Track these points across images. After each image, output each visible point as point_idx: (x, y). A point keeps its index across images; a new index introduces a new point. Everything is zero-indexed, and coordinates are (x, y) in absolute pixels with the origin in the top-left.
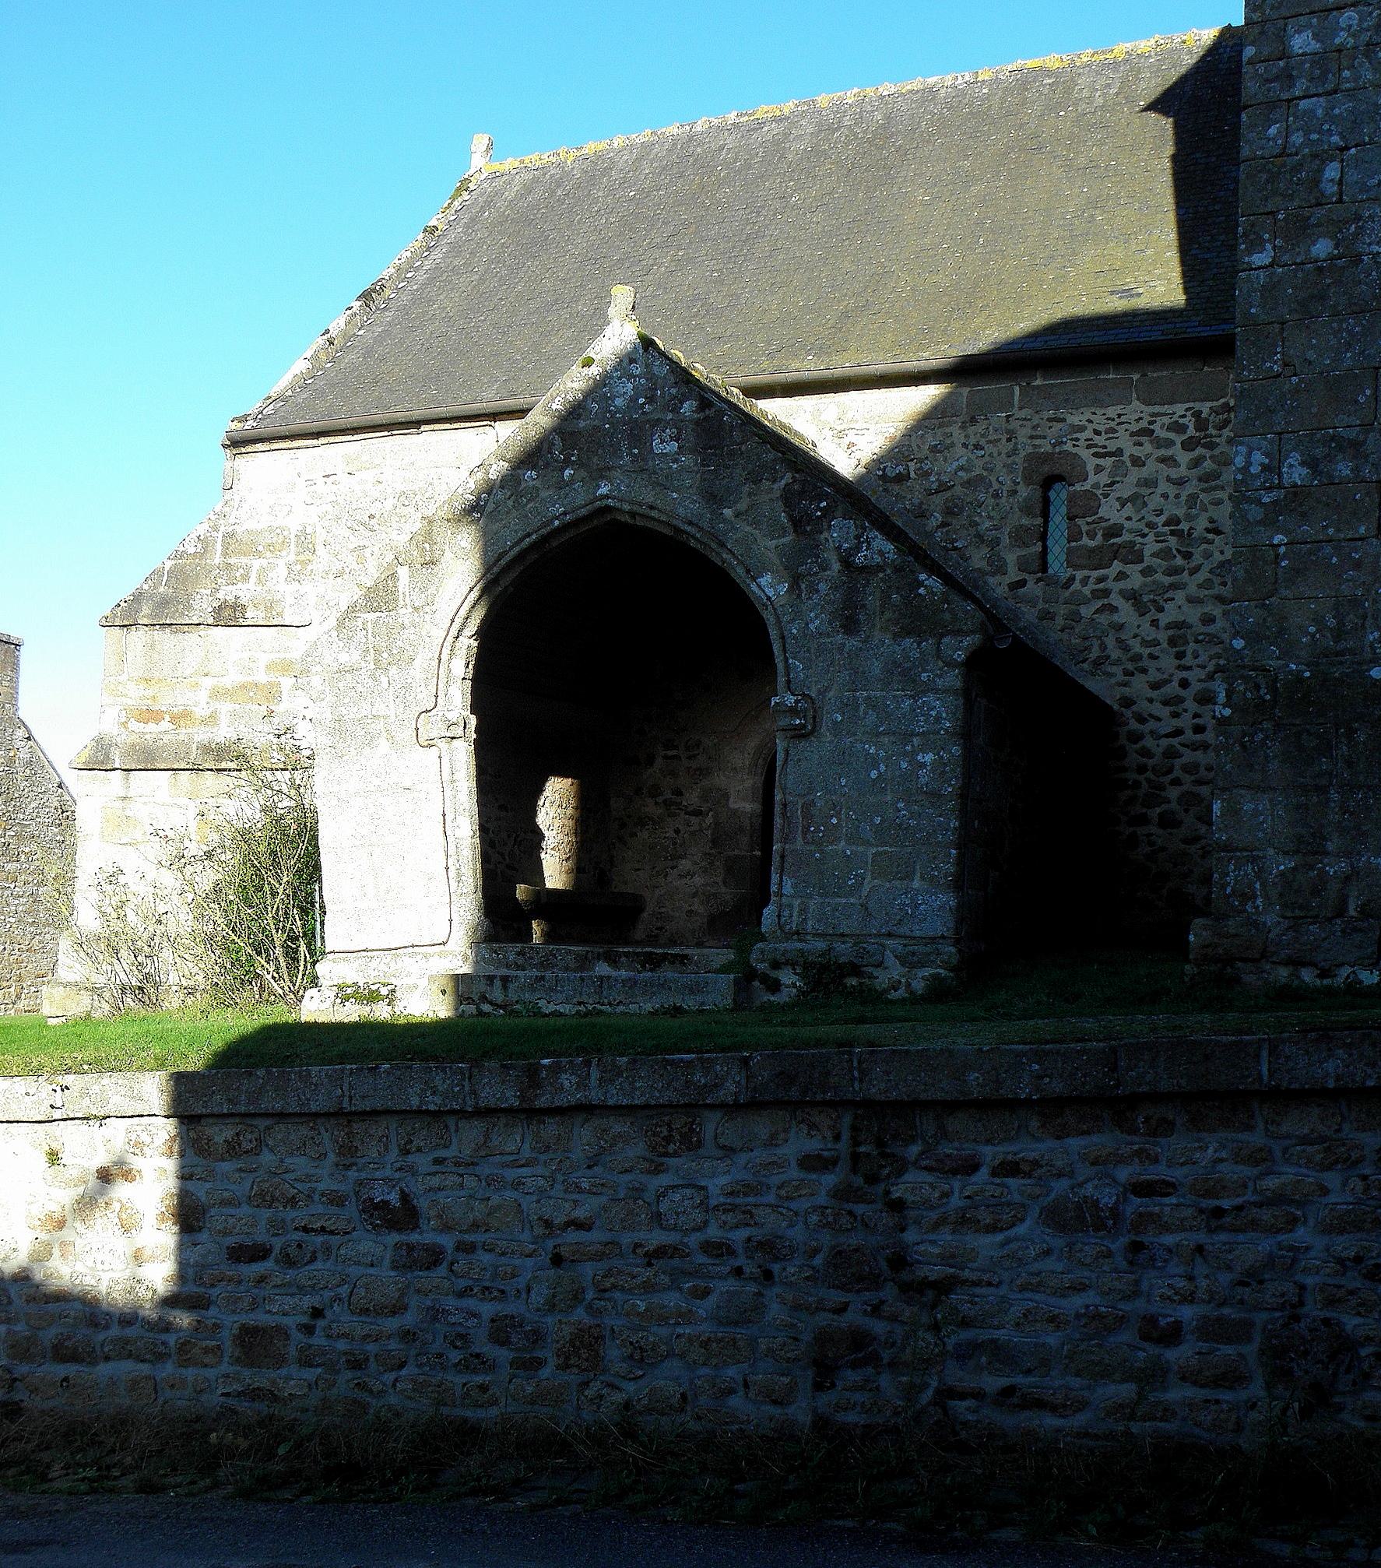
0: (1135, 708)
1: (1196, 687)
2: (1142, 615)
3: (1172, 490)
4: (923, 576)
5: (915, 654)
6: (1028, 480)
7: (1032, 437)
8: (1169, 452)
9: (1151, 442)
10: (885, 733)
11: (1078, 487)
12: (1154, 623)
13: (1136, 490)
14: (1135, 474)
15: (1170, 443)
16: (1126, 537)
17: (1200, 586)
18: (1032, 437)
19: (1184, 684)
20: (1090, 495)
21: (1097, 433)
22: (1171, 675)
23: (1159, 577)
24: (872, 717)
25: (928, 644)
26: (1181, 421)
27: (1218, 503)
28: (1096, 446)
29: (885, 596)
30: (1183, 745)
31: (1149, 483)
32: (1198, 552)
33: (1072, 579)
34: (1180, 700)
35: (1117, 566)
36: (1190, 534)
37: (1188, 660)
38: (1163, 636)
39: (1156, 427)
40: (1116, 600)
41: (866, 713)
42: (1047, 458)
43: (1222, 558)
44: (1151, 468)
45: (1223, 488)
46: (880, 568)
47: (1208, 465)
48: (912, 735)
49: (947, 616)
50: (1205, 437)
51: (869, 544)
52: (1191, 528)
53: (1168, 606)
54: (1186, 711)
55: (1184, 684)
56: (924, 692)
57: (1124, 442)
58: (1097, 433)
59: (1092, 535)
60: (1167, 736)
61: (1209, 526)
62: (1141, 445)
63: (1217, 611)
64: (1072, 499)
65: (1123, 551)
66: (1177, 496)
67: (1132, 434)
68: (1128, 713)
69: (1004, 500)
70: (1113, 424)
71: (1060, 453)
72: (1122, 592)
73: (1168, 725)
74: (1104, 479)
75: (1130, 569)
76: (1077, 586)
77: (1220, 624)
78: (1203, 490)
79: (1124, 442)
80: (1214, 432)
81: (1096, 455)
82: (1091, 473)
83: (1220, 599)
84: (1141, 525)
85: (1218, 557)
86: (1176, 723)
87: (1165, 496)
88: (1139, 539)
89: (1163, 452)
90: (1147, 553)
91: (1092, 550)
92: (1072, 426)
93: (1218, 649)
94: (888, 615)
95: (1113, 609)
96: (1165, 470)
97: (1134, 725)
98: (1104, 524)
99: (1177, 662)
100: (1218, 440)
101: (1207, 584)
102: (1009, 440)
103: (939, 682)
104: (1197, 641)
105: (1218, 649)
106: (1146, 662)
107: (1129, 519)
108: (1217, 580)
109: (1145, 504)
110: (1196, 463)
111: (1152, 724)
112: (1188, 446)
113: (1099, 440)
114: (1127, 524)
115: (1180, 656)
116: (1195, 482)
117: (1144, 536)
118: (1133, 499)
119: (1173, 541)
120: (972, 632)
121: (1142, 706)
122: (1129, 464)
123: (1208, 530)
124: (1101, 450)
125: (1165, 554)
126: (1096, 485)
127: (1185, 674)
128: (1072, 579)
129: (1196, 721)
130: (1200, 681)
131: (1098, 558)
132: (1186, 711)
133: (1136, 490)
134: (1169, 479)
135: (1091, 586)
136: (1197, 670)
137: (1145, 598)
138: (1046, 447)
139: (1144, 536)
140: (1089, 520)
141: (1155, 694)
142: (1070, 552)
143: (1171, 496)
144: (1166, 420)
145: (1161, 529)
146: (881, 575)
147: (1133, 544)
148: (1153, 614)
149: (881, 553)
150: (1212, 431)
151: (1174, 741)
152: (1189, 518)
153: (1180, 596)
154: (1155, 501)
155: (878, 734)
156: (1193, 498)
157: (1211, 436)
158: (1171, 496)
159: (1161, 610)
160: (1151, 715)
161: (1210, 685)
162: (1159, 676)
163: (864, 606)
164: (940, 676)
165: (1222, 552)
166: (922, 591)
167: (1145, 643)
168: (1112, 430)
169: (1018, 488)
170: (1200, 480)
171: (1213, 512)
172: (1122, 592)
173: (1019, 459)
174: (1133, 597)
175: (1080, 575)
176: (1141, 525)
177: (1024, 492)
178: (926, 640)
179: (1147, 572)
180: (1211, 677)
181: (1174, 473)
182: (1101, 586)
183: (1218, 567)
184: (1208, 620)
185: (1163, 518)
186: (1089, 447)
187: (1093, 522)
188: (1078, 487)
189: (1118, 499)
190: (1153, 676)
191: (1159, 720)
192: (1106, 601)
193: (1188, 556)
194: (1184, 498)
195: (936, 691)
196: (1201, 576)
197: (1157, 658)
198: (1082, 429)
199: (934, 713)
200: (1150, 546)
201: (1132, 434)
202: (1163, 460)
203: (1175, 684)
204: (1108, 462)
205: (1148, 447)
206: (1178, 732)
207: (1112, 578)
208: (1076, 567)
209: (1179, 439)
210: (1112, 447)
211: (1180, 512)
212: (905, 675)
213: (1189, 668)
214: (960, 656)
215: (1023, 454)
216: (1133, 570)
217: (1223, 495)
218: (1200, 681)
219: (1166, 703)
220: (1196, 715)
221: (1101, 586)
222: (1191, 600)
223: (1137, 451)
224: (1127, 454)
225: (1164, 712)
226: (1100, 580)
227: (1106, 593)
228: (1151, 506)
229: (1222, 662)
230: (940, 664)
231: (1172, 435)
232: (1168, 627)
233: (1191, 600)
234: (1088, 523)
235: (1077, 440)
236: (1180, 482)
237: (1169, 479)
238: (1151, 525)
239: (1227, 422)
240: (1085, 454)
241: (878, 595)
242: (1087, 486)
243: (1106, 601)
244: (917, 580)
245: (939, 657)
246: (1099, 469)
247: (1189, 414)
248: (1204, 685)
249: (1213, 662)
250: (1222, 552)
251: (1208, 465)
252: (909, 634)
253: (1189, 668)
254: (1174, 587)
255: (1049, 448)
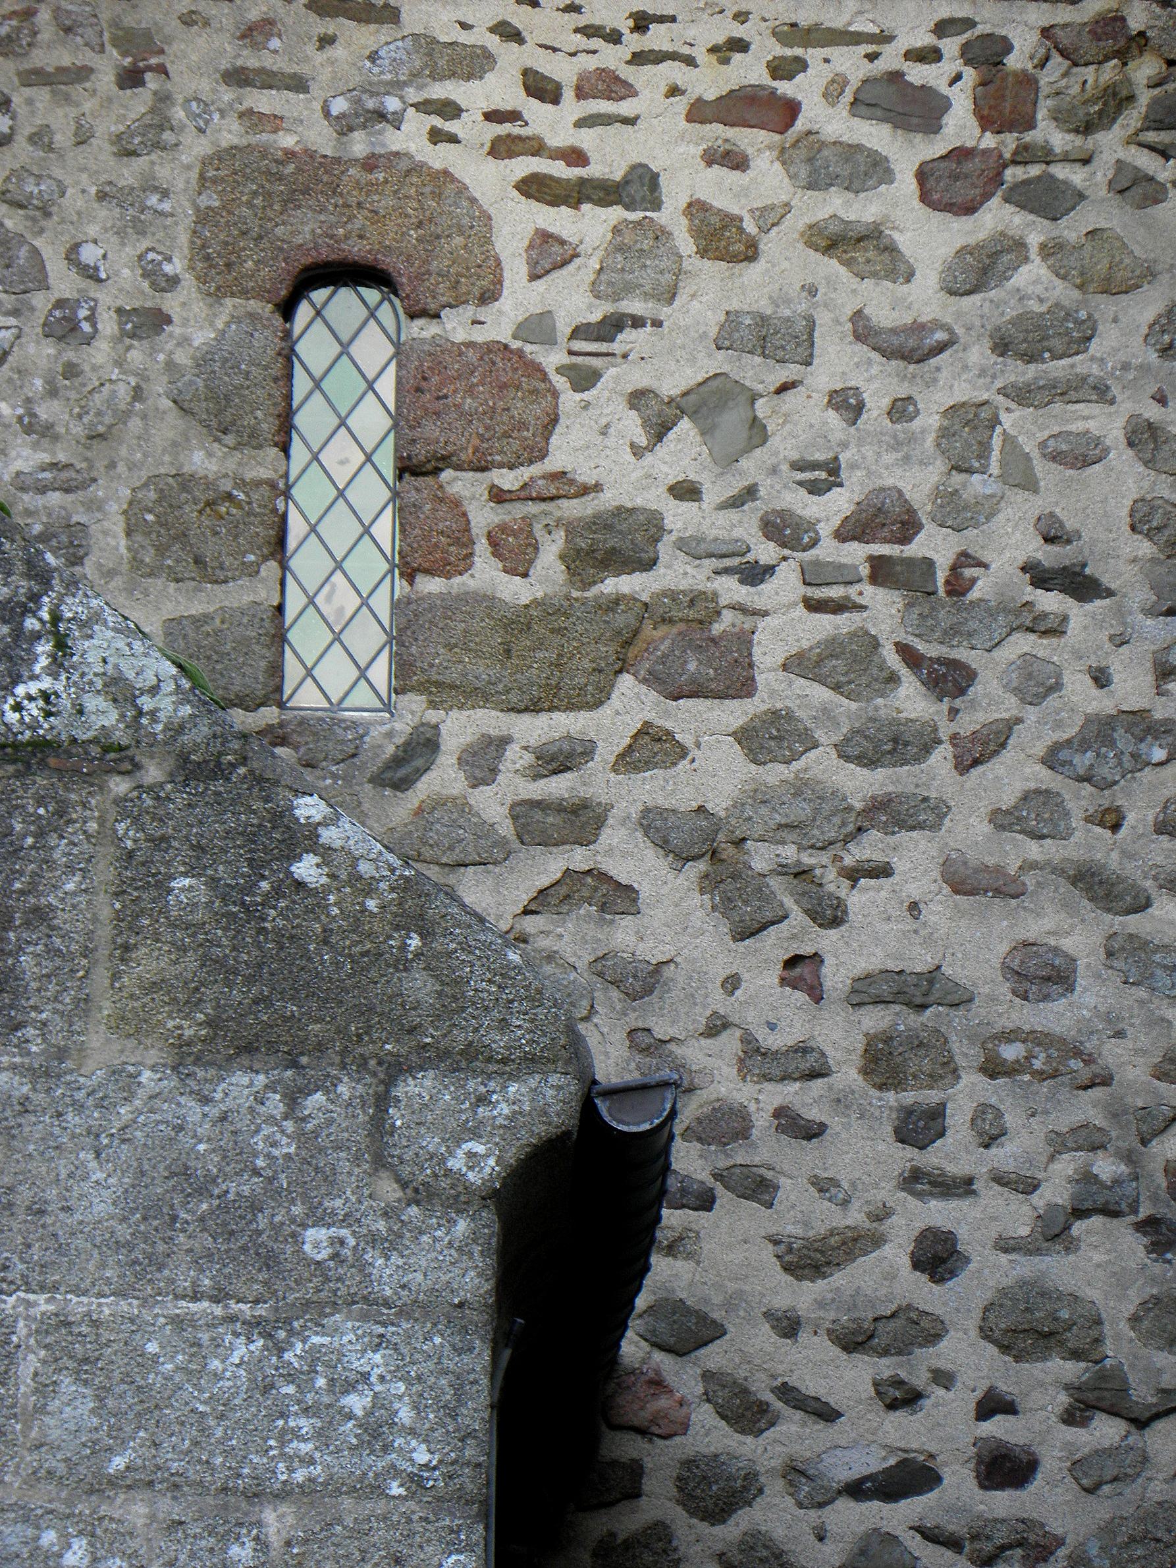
0: (713, 1356)
1: (988, 1273)
2: (746, 932)
3: (879, 384)
4: (309, 808)
5: (275, 1142)
6: (219, 271)
7: (238, 77)
8: (862, 210)
9: (783, 155)
10: (137, 1482)
11: (456, 326)
12: (800, 969)
13: (719, 362)
14: (710, 294)
15: (869, 170)
16: (674, 573)
17: (1003, 820)
18: (238, 77)
19: (937, 1257)
20: (508, 368)
21: (542, 89)
22: (881, 1215)
23: (823, 764)
24: (73, 1409)
25: (334, 1104)
26: (917, 74)
27: (1081, 455)
28: (537, 148)
29: (140, 880)
30: (931, 1535)
31: (778, 339)
32: (994, 667)
33: (422, 747)
34: (923, 1330)
35: (631, 703)
36: (957, 587)
37: (954, 1152)
38: (841, 1035)
39: (804, 89)
40: (623, 854)
41: (45, 1389)
42: (310, 177)
43: (1100, 703)
44: (783, 271)
45: (1102, 393)
46: (115, 756)
47: (1033, 281)
48: (255, 1496)
49: (419, 986)
50: (1023, 156)
51: (61, 644)
52: (965, 559)
53: (861, 900)
54: (944, 1379)
55: (937, 1257)
56: (317, 1310)
57: (659, 138)
58: (542, 89)
59: (516, 554)
60: (856, 1490)
61: (1049, 556)
62: (735, 161)
63: (1080, 935)
64: (423, 383)
65: (661, 638)
66: (901, 410)
67: (699, 113)
68: (684, 1378)
69: (101, 353)
70: (612, 57)
71: (370, 163)
72: (654, 825)
73: (867, 1441)
74: (572, 299)
75: (689, 719)
76: (444, 777)
77: (1093, 995)
78: (1021, 395)
79: (659, 138)
80: (1060, 140)
81: (534, 188)
82: (515, 270)
83: (1096, 886)
84: (744, 528)
85: (1081, 698)
86: (906, 1432)
87: (847, 403)
88: (730, 589)
89: (836, 205)
90: (769, 651)
91: (518, 623)
92: (427, 44)
93: (1087, 1108)
94: (150, 962)
95: (617, 897)
96: (846, 289)
97: (708, 1433)
98: (572, 509)
99: (906, 1157)
100: (1076, 176)
101: (1030, 816)
102: (131, 78)
103: (385, 1271)
104: (993, 1069)
105: (1087, 1108)
106: (766, 1149)
107: (686, 491)
108: (1080, 801)
109: (758, 433)
110: (980, 270)
111: (792, 1434)
112: (950, 186)
113: (552, 123)
114: (679, 517)
115: (918, 1128)
116: (979, 354)
117: (755, 574)
118: (706, 403)
119: (883, 612)
120: (532, 1062)
121: (749, 1351)
122: (685, 244)
123: (1040, 577)
124: (559, 169)
125: (844, 665)
126: (537, 327)
127: (939, 1213)
128: (422, 747)
129: (997, 1427)
130: (1006, 1246)
131: (549, 661)
132: (944, 1379)
133: (719, 362)
134: (863, 330)
135: (516, 782)
136: (992, 1198)
137: (761, 857)
138: (305, 128)
139: (755, 574)
140: (508, 480)
141: (804, 1296)
142: (407, 629)
143: (877, 403)
144: (850, 63)
145: (828, 550)
146: (120, 786)
147: (702, 607)
148: (795, 932)
149: (119, 690)
150: (1049, 133)
151: (898, 1516)
152: (956, 512)
153: (915, 859)
154: (801, 423)
155: (102, 1486)
156: (969, 427)
157: (1047, 156)
158: (877, 403)
159: (831, 916)
160: (786, 1392)
161: (1058, 1270)
162: (826, 1217)
163: (41, 915)
164: (389, 1244)
165: (1101, 678)
166: (307, 869)
167: (756, 1059)
168: (611, 85)
169: (171, 303)
170: (1002, 347)
171: (1056, 494)
172: (654, 825)
173: (179, 168)
174: (705, 847)
175: (460, 728)
176: (744, 528)
177: (199, 323)
178: (327, 1085)
179: (768, 738)
180: (1055, 1232)
181: (885, 305)
182: (558, 786)
183: (1082, 743)
184: (1040, 974)
185: (837, 505)
186: (501, 149)
187: (524, 494)
188: (456, 326)
189: (637, 398)
190: (800, 1212)
191: (827, 1414)
192: (579, 858)
193: (950, 681)
194: (929, 420)
195: (369, 1305)
196: (1014, 774)
197: (812, 1132)
198: (474, 64)
199: (357, 1403)
200: (783, 627)
201: (699, 113)
202: (834, 241)
203: (896, 1253)
204: (590, 226)
205: (767, 178)
206: (908, 1478)
207: (606, 753)
208: (441, 692)
209: (906, 154)
210: (609, 156)
211: (918, 483)
212: (223, 1230)
213: (963, 1187)
214: (480, 1161)
215: (195, 148)
216: (709, 724)
217: (1105, 424)
218: (1006, 1246)
219: (854, 1342)
220: (992, 1405)
221: (558, 786)
222: (963, 881)
223: (721, 190)
224: (674, 197)
225: (849, 1380)
226: (558, 759)
227: (581, 821)
228: (784, 444)
229: (1106, 1167)
230: (388, 1190)
231: (875, 136)
232: (865, 992)
233: (963, 881)
234: (498, 496)
235: (450, 110)
236: (914, 348)
237: (863, 330)
238: (785, 530)
239: (1116, 100)
240: (489, 181)
241: (105, 872)
242: (499, 324)
243: (579, 858)
244: (282, 818)
245: (380, 1162)
246: (549, 255)
247: (951, 46)
248: (1023, 1267)
249: (1067, 1166)
250: (1101, 678)
251: (1033, 281)
252: (246, 1050)
253: (963, 1187)
254: (888, 813)
255: (320, 138)
